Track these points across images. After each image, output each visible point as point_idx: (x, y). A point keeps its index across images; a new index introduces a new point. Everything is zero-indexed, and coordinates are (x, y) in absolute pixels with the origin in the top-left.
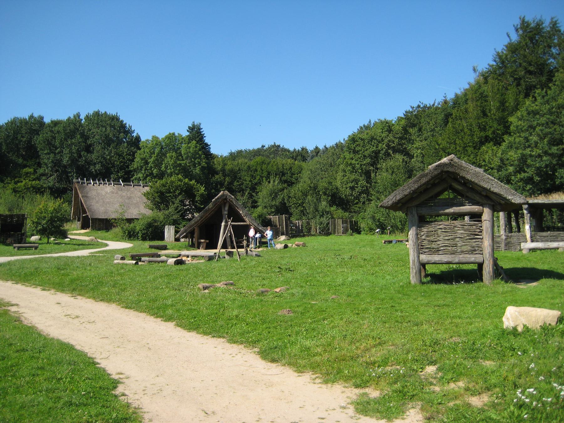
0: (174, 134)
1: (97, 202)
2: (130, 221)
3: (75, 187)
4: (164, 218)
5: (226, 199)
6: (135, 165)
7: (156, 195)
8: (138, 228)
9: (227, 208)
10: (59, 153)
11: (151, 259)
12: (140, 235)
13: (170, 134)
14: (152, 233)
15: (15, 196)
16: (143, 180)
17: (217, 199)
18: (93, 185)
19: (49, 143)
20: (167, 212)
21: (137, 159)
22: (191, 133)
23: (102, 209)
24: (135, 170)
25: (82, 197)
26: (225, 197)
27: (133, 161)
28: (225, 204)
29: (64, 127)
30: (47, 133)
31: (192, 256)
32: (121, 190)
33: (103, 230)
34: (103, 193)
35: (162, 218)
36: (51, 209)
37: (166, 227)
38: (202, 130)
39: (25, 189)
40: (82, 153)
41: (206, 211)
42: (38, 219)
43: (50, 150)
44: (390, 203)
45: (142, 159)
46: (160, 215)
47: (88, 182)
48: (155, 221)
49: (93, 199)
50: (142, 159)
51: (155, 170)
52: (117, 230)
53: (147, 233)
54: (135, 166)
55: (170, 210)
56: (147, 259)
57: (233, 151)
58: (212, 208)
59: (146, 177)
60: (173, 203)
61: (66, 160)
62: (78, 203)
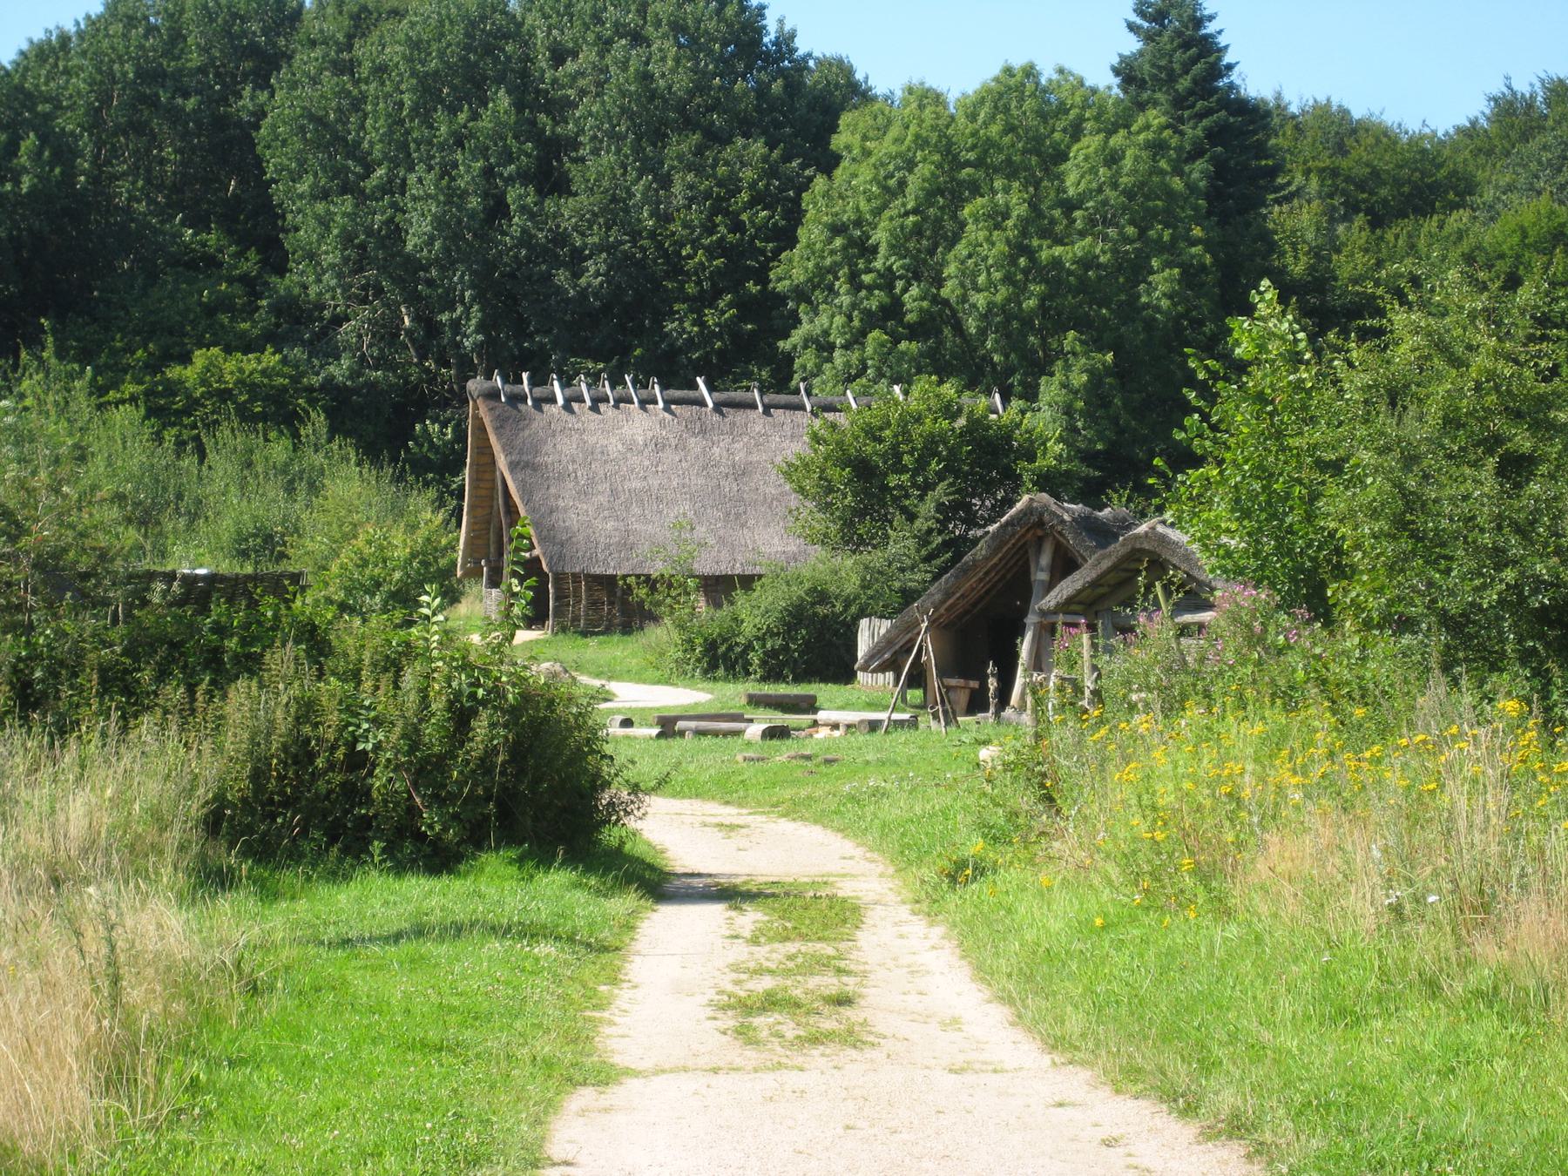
0: (1030, 72)
1: (583, 494)
2: (718, 587)
3: (477, 418)
4: (865, 586)
5: (1041, 524)
6: (792, 270)
7: (834, 473)
8: (748, 629)
9: (1045, 559)
10: (386, 188)
11: (704, 725)
12: (755, 658)
13: (1008, 71)
14: (807, 646)
15: (158, 438)
16: (846, 347)
17: (1007, 523)
18: (567, 407)
19: (330, 137)
20: (876, 558)
21: (810, 232)
22: (1149, 37)
23: (607, 528)
24: (801, 294)
25: (513, 466)
26: (1034, 518)
27: (787, 238)
28: (1040, 541)
29: (415, 45)
30: (315, 81)
31: (849, 726)
32: (703, 431)
33: (608, 631)
34: (615, 446)
35: (852, 585)
36: (401, 553)
37: (864, 623)
38: (1211, 28)
39: (209, 395)
40: (511, 196)
41: (966, 571)
42: (349, 591)
43: (338, 172)
44: (1052, 603)
45: (837, 229)
46: (844, 571)
47: (538, 391)
48: (821, 596)
49: (561, 477)
50: (837, 229)
51: (914, 291)
52: (662, 635)
53: (785, 648)
54: (799, 275)
55: (892, 549)
56: (693, 724)
57: (1522, 87)
58: (987, 559)
59: (863, 333)
60: (912, 517)
61: (418, 231)
62: (492, 498)
